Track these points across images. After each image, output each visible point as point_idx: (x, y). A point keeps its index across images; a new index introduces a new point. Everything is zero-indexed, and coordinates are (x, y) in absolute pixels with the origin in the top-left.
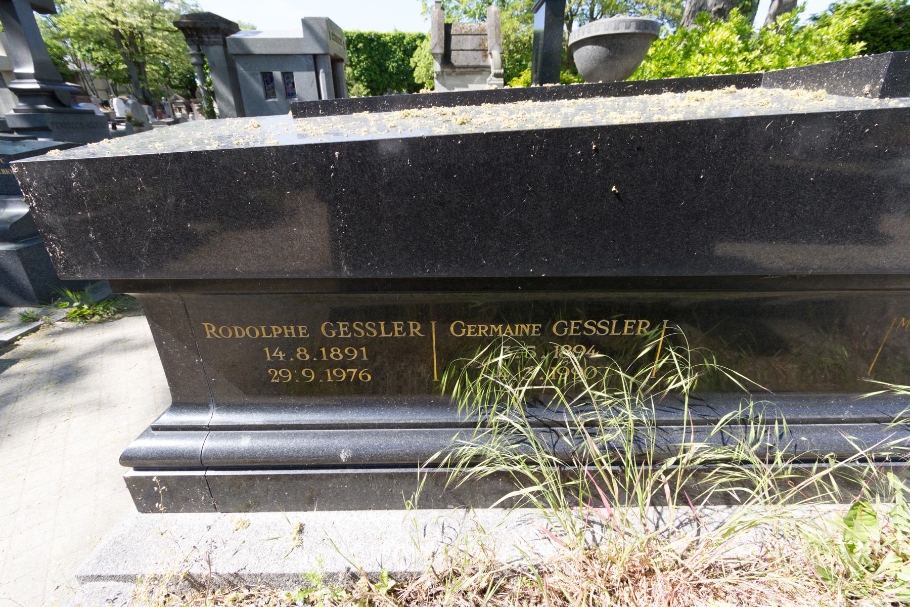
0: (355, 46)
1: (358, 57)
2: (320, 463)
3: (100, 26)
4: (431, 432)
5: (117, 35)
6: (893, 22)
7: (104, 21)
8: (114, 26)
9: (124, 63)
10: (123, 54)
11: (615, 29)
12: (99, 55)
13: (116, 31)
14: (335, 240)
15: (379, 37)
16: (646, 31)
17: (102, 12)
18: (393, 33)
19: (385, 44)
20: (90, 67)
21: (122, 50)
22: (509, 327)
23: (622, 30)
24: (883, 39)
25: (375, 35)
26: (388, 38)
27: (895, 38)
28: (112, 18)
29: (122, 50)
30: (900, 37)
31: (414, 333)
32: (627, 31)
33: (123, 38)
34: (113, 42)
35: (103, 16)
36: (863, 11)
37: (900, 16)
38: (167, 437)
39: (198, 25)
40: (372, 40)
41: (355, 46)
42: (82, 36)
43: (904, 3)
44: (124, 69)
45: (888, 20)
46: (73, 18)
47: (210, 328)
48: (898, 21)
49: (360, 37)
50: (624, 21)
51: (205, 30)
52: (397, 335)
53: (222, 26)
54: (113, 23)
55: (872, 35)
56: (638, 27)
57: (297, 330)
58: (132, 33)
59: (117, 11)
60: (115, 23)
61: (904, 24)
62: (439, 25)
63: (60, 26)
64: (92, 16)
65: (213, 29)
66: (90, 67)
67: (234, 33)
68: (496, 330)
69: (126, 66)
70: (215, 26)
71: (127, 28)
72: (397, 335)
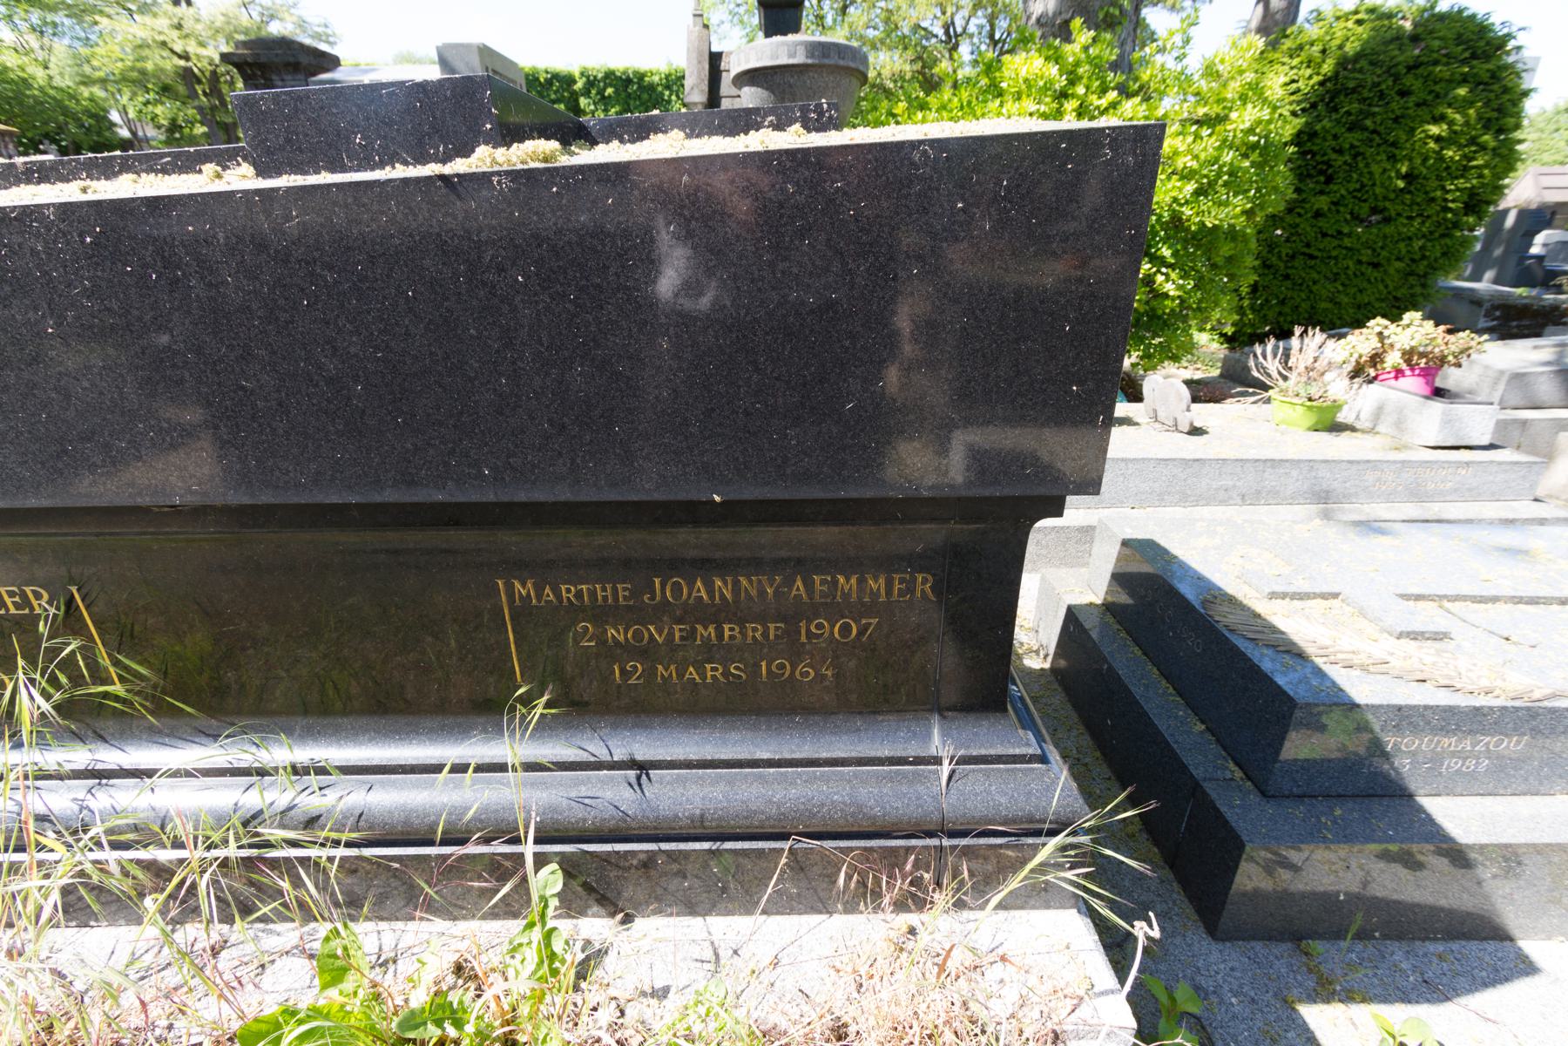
0: (601, 92)
1: (606, 110)
2: (829, 829)
3: (161, 63)
4: (856, 775)
5: (188, 76)
6: (1406, 41)
7: (166, 53)
8: (182, 63)
9: (202, 124)
10: (200, 109)
11: (772, 58)
12: (163, 111)
13: (188, 71)
14: (1023, 417)
15: (641, 76)
16: (826, 61)
17: (162, 38)
18: (664, 69)
19: (652, 88)
20: (151, 132)
21: (196, 103)
22: (547, 590)
23: (784, 60)
24: (1388, 71)
25: (636, 73)
26: (656, 79)
27: (1409, 68)
28: (178, 48)
29: (196, 103)
30: (1416, 66)
31: (923, 591)
32: (791, 61)
33: (199, 82)
34: (182, 89)
35: (164, 44)
36: (1359, 22)
37: (1420, 30)
38: (416, 786)
39: (263, 59)
40: (629, 81)
41: (601, 92)
42: (137, 80)
43: (1432, 7)
44: (204, 134)
45: (1398, 38)
46: (117, 48)
47: (38, 596)
48: (1415, 38)
49: (610, 76)
50: (801, 43)
51: (276, 63)
52: (13, 610)
53: (304, 60)
54: (180, 57)
55: (1372, 63)
56: (810, 54)
57: (615, 591)
58: (214, 73)
59: (186, 36)
60: (185, 56)
61: (1423, 45)
62: (700, 54)
63: (95, 63)
64: (143, 45)
65: (287, 64)
66: (151, 132)
67: (327, 70)
68: (847, 588)
69: (205, 129)
70: (291, 60)
71: (204, 64)
72: (13, 610)
